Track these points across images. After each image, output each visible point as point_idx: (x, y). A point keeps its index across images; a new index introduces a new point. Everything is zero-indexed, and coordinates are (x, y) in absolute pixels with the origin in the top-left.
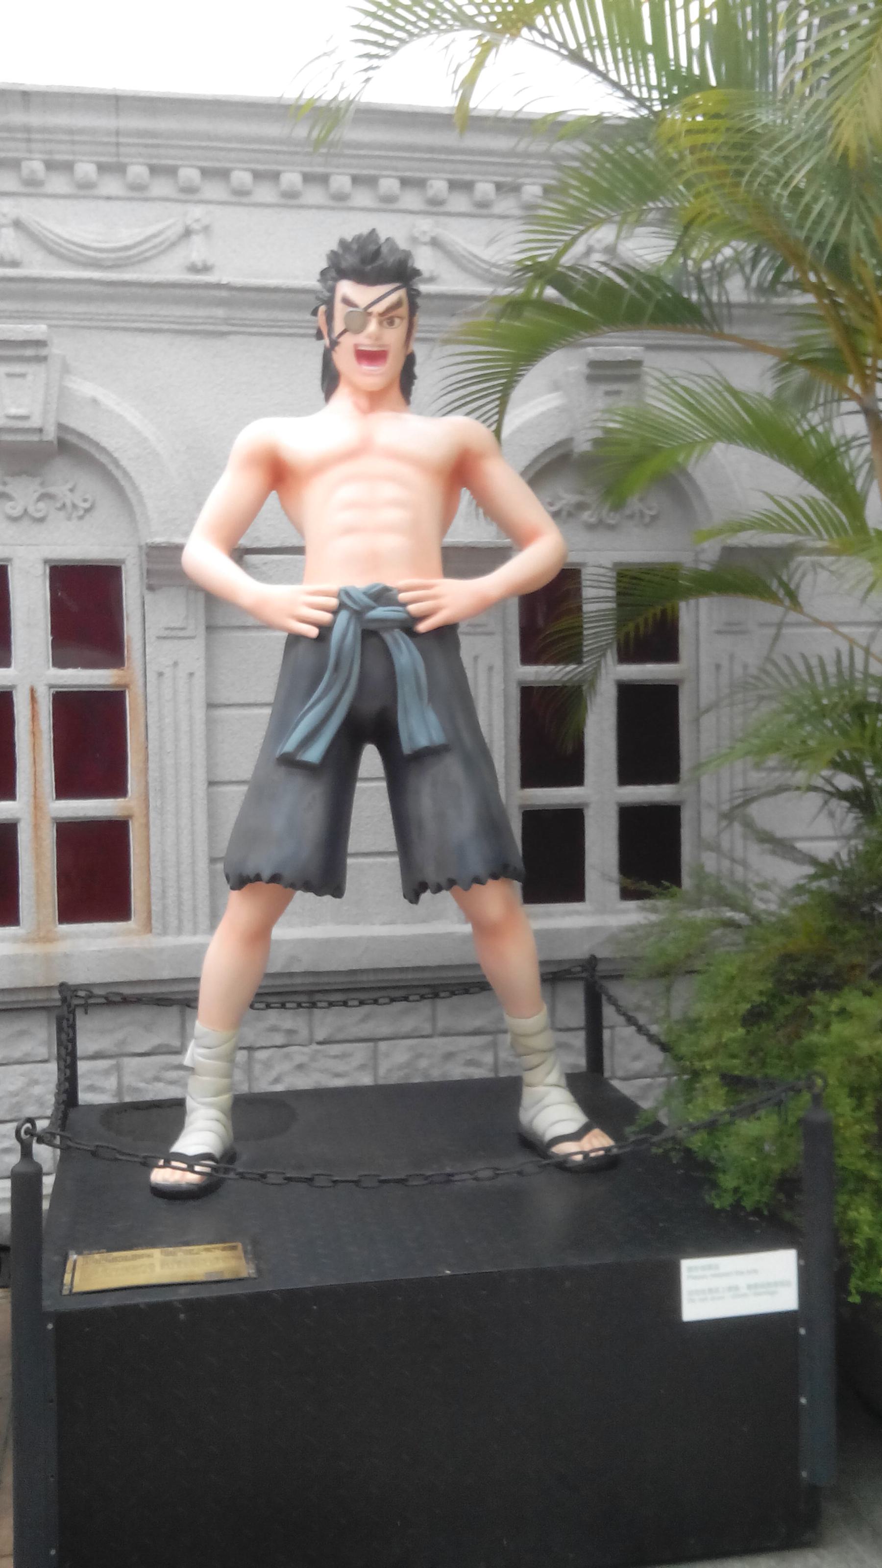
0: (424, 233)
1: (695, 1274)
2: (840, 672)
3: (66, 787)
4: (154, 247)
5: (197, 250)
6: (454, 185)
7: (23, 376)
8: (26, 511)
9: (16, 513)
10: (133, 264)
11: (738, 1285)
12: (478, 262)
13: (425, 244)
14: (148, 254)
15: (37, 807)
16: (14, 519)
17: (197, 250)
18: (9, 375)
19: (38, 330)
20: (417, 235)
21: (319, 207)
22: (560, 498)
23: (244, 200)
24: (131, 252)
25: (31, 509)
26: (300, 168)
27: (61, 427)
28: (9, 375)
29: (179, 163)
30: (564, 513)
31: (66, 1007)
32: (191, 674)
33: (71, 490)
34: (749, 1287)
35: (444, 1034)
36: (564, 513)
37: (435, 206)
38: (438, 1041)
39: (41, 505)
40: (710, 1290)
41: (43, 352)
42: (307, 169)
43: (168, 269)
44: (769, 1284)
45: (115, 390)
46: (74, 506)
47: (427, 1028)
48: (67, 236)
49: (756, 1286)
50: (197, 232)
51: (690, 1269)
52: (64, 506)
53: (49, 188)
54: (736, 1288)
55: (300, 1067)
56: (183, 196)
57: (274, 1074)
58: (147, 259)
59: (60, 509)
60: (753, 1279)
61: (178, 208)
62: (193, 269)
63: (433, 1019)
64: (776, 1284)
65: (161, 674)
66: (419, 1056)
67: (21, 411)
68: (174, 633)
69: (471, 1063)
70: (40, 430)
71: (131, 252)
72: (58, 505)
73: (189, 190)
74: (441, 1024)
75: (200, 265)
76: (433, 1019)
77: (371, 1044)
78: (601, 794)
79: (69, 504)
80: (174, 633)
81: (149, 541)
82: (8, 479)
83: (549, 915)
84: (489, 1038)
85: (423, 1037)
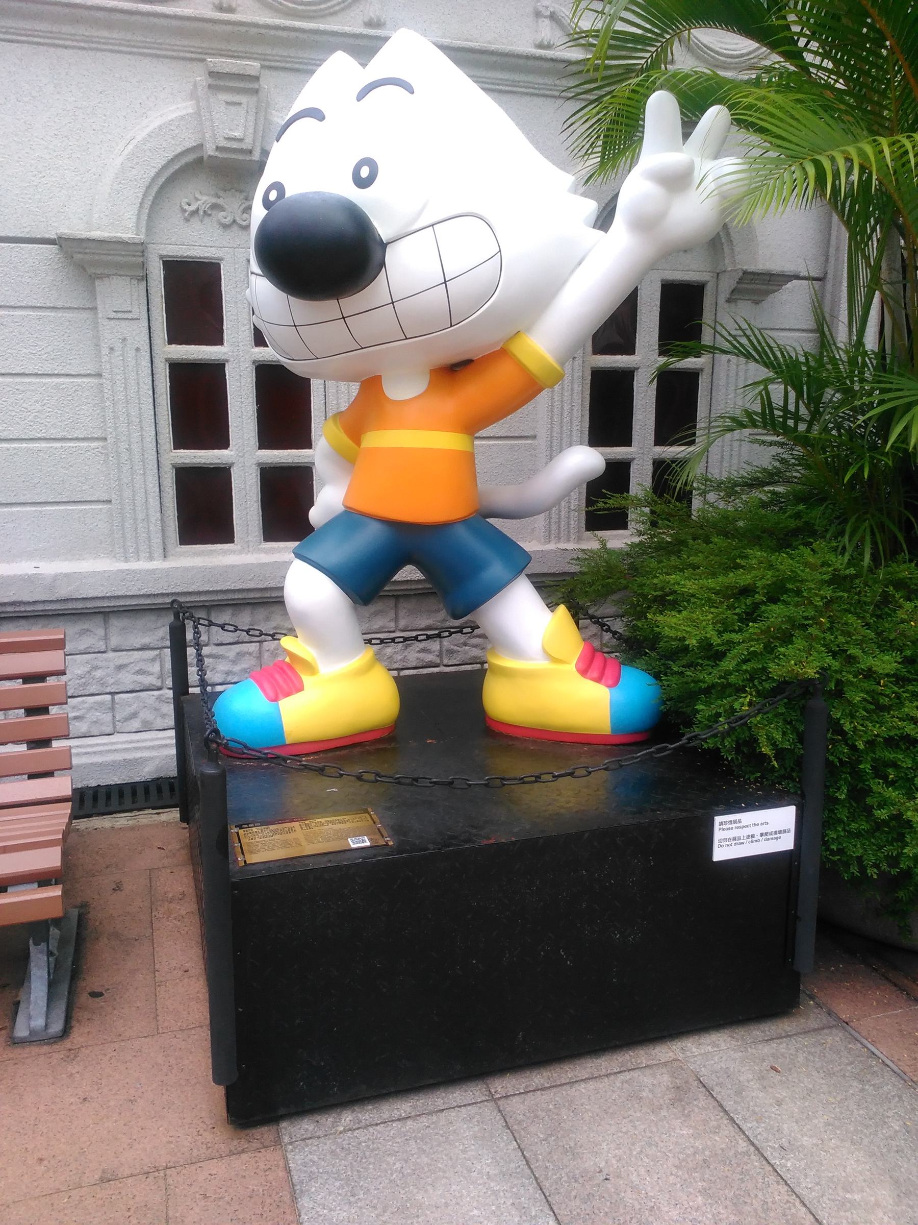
0: (547, 7)
1: (724, 827)
2: (785, 361)
3: (661, 439)
7: (240, 104)
8: (234, 221)
9: (228, 221)
10: (323, 16)
11: (756, 832)
13: (546, 17)
14: (337, 8)
16: (225, 227)
19: (252, 66)
20: (541, 9)
22: (197, 200)
25: (238, 219)
30: (201, 212)
32: (138, 350)
34: (762, 835)
35: (115, 650)
36: (201, 212)
38: (111, 655)
40: (734, 839)
44: (776, 833)
47: (101, 646)
49: (766, 834)
51: (721, 824)
54: (753, 836)
60: (764, 829)
63: (106, 638)
64: (780, 832)
66: (96, 668)
67: (237, 134)
68: (120, 315)
69: (140, 672)
70: (250, 152)
74: (114, 641)
76: (106, 638)
78: (244, 455)
80: (120, 315)
81: (745, 268)
84: (157, 652)
85: (99, 652)
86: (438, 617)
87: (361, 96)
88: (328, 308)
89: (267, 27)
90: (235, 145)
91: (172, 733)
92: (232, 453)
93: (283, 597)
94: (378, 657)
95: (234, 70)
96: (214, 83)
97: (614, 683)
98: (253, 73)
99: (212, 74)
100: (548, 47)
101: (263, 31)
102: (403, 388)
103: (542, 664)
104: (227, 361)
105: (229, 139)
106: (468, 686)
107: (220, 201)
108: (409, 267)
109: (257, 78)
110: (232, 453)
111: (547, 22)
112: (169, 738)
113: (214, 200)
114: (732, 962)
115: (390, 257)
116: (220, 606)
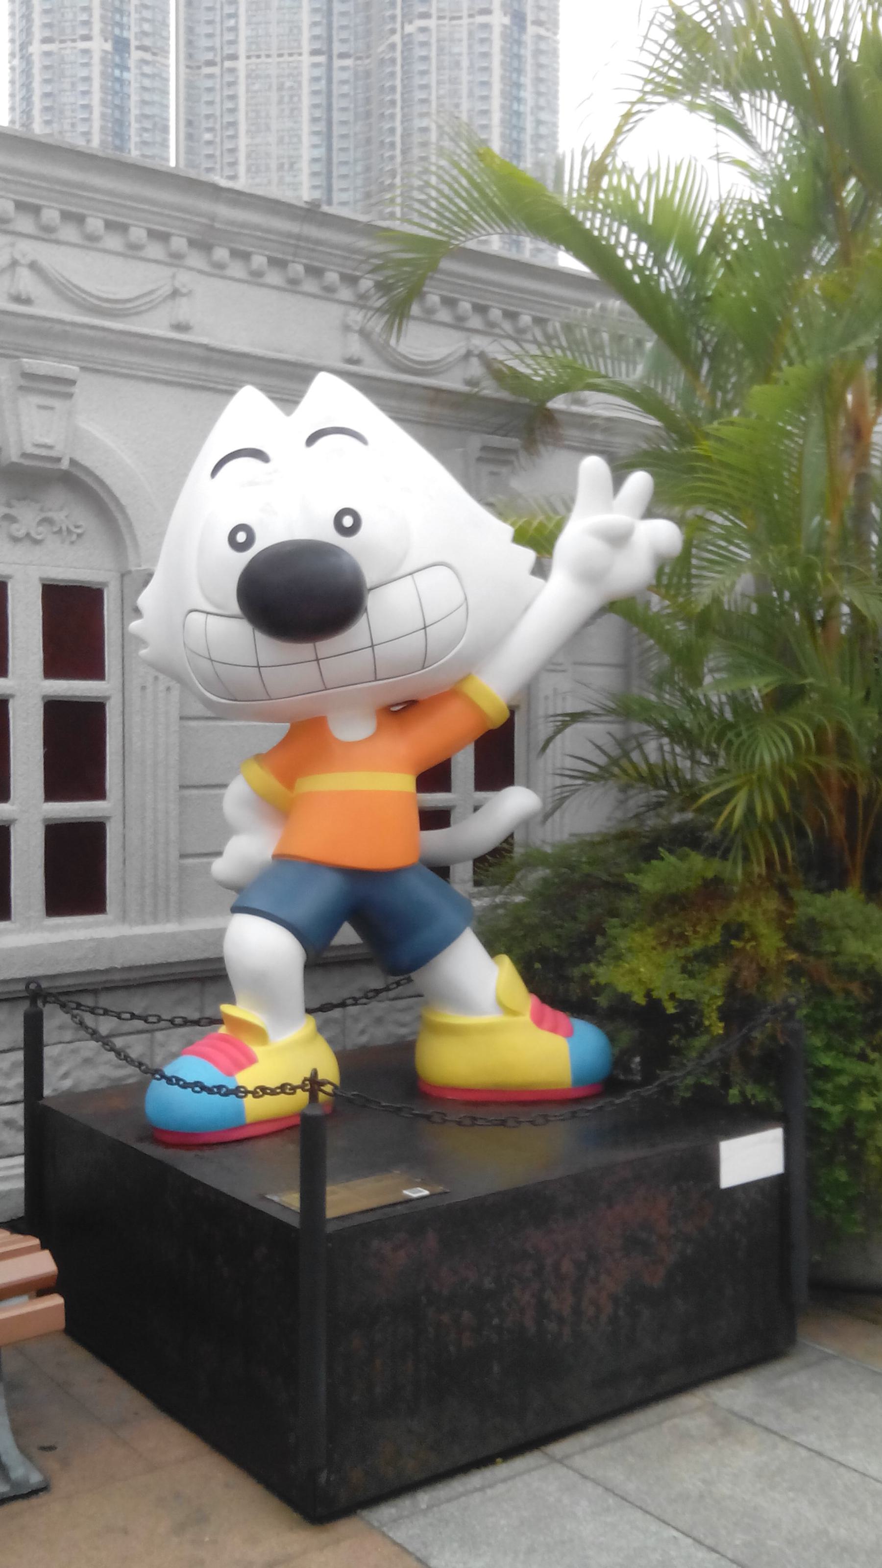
4: (146, 303)
5: (183, 310)
6: (110, 225)
7: (52, 408)
8: (28, 535)
9: (21, 533)
12: (77, 292)
14: (143, 308)
15: (30, 810)
16: (15, 540)
17: (183, 310)
18: (40, 407)
19: (69, 369)
21: (315, 296)
23: (95, 245)
24: (129, 305)
26: (305, 261)
27: (73, 462)
28: (40, 407)
29: (173, 231)
31: (37, 999)
33: (67, 517)
37: (46, 234)
39: (41, 529)
41: (23, 382)
42: (110, 217)
43: (155, 325)
45: (102, 427)
46: (69, 531)
48: (75, 282)
50: (184, 295)
52: (60, 531)
53: (229, 272)
55: (87, 1061)
56: (87, 243)
57: (63, 1069)
58: (137, 314)
59: (55, 533)
61: (167, 272)
62: (18, 299)
65: (143, 688)
70: (58, 460)
71: (129, 305)
72: (56, 529)
73: (176, 257)
75: (355, 358)
77: (147, 1035)
79: (64, 528)
82: (14, 502)
83: (57, 928)
86: (373, 979)
87: (312, 440)
88: (305, 650)
89: (74, 324)
90: (44, 452)
91: (21, 1160)
92: (14, 808)
93: (225, 969)
94: (320, 1029)
95: (51, 373)
96: (26, 384)
97: (568, 1034)
98: (72, 377)
99: (26, 375)
100: (28, 301)
101: (68, 328)
102: (352, 728)
103: (493, 1017)
104: (12, 696)
105: (38, 446)
106: (403, 1053)
107: (13, 512)
108: (393, 612)
109: (72, 383)
110: (14, 808)
111: (356, 337)
112: (18, 1166)
113: (6, 510)
114: (739, 1306)
115: (372, 602)
116: (111, 988)
